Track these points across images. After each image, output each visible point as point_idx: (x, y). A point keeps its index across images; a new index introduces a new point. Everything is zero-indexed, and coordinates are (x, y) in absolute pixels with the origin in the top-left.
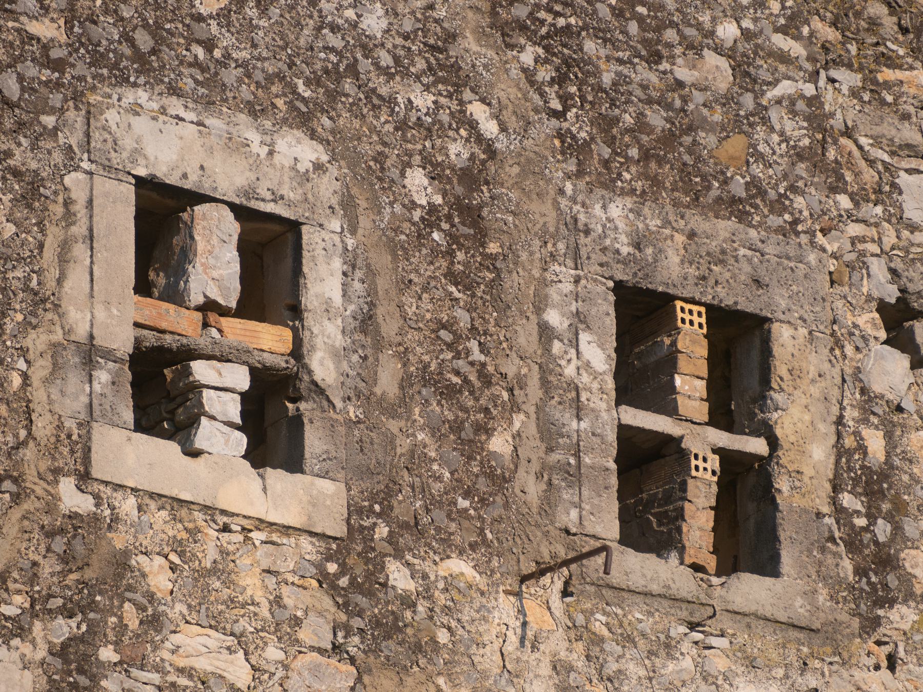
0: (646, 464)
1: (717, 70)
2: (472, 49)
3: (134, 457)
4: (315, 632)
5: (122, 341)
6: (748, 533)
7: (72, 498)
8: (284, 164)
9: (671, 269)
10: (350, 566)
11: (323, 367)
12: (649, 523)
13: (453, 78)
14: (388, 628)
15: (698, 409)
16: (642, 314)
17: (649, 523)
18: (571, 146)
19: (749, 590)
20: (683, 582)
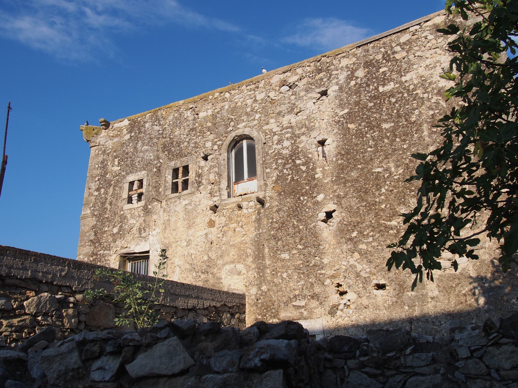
8: (141, 174)
10: (145, 209)
19: (185, 192)
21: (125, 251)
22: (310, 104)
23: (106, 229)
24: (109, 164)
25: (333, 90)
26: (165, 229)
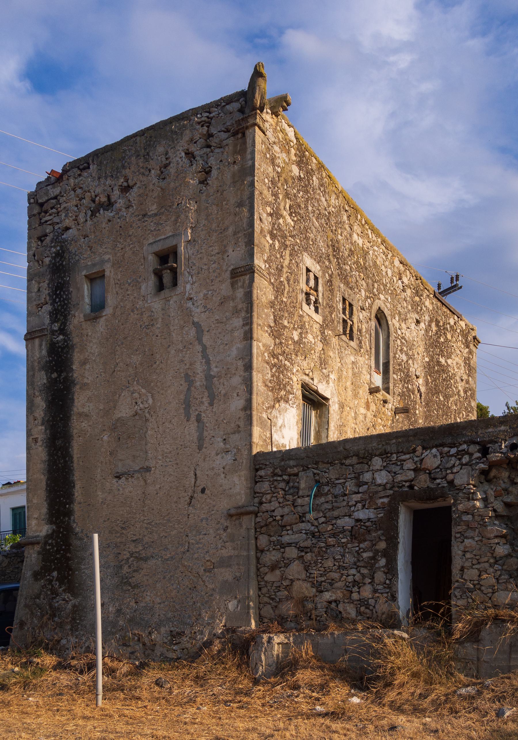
0: (344, 321)
1: (348, 268)
2: (331, 257)
3: (305, 307)
4: (319, 338)
5: (305, 291)
6: (351, 338)
7: (301, 313)
9: (346, 296)
11: (320, 300)
12: (345, 333)
13: (330, 262)
14: (325, 340)
15: (348, 316)
16: (344, 300)
17: (345, 333)
18: (339, 275)
20: (347, 341)
21: (307, 379)
22: (413, 326)
23: (286, 323)
24: (281, 196)
25: (422, 325)
26: (339, 379)
